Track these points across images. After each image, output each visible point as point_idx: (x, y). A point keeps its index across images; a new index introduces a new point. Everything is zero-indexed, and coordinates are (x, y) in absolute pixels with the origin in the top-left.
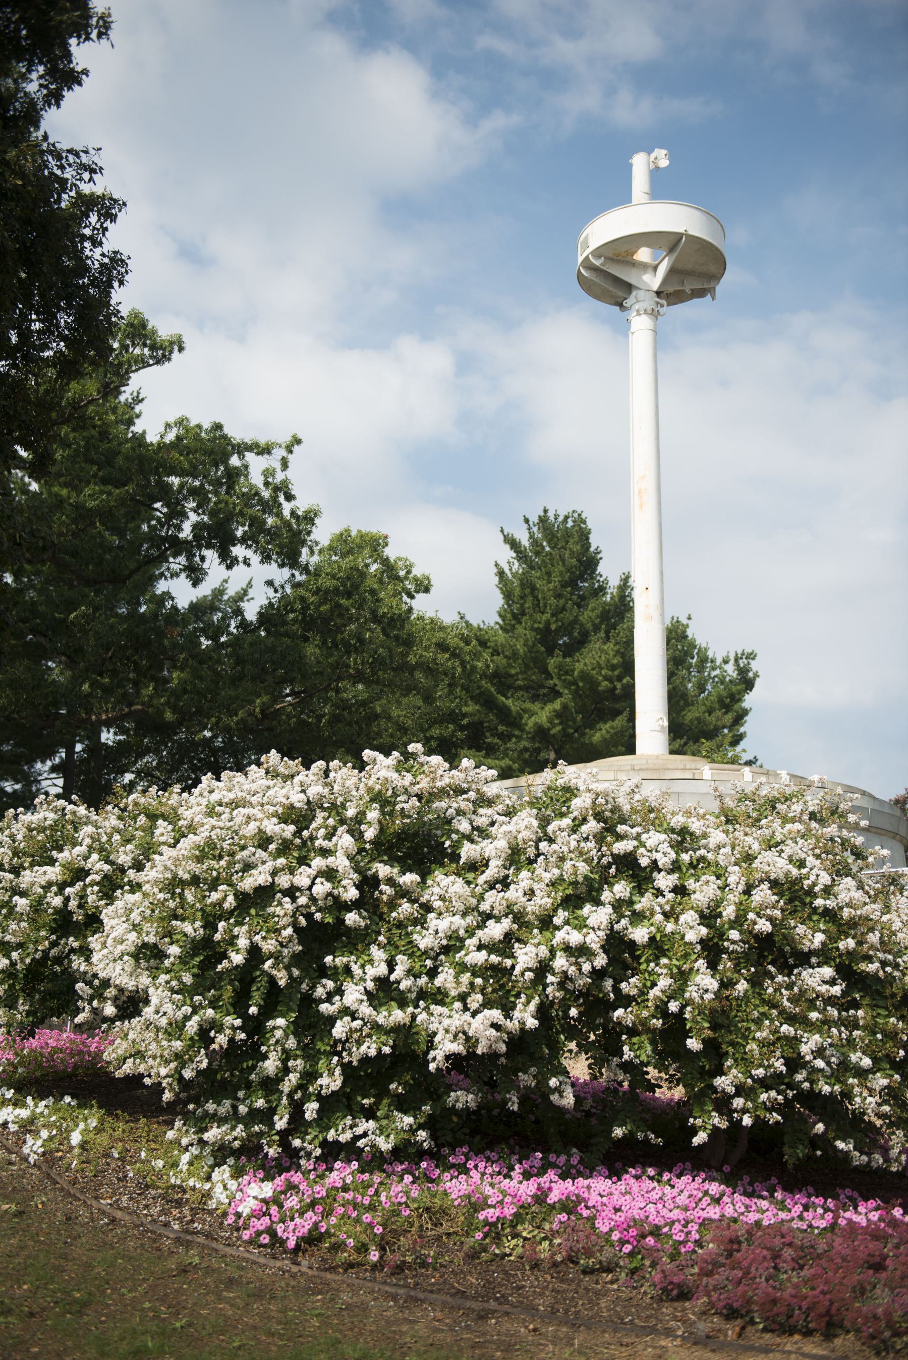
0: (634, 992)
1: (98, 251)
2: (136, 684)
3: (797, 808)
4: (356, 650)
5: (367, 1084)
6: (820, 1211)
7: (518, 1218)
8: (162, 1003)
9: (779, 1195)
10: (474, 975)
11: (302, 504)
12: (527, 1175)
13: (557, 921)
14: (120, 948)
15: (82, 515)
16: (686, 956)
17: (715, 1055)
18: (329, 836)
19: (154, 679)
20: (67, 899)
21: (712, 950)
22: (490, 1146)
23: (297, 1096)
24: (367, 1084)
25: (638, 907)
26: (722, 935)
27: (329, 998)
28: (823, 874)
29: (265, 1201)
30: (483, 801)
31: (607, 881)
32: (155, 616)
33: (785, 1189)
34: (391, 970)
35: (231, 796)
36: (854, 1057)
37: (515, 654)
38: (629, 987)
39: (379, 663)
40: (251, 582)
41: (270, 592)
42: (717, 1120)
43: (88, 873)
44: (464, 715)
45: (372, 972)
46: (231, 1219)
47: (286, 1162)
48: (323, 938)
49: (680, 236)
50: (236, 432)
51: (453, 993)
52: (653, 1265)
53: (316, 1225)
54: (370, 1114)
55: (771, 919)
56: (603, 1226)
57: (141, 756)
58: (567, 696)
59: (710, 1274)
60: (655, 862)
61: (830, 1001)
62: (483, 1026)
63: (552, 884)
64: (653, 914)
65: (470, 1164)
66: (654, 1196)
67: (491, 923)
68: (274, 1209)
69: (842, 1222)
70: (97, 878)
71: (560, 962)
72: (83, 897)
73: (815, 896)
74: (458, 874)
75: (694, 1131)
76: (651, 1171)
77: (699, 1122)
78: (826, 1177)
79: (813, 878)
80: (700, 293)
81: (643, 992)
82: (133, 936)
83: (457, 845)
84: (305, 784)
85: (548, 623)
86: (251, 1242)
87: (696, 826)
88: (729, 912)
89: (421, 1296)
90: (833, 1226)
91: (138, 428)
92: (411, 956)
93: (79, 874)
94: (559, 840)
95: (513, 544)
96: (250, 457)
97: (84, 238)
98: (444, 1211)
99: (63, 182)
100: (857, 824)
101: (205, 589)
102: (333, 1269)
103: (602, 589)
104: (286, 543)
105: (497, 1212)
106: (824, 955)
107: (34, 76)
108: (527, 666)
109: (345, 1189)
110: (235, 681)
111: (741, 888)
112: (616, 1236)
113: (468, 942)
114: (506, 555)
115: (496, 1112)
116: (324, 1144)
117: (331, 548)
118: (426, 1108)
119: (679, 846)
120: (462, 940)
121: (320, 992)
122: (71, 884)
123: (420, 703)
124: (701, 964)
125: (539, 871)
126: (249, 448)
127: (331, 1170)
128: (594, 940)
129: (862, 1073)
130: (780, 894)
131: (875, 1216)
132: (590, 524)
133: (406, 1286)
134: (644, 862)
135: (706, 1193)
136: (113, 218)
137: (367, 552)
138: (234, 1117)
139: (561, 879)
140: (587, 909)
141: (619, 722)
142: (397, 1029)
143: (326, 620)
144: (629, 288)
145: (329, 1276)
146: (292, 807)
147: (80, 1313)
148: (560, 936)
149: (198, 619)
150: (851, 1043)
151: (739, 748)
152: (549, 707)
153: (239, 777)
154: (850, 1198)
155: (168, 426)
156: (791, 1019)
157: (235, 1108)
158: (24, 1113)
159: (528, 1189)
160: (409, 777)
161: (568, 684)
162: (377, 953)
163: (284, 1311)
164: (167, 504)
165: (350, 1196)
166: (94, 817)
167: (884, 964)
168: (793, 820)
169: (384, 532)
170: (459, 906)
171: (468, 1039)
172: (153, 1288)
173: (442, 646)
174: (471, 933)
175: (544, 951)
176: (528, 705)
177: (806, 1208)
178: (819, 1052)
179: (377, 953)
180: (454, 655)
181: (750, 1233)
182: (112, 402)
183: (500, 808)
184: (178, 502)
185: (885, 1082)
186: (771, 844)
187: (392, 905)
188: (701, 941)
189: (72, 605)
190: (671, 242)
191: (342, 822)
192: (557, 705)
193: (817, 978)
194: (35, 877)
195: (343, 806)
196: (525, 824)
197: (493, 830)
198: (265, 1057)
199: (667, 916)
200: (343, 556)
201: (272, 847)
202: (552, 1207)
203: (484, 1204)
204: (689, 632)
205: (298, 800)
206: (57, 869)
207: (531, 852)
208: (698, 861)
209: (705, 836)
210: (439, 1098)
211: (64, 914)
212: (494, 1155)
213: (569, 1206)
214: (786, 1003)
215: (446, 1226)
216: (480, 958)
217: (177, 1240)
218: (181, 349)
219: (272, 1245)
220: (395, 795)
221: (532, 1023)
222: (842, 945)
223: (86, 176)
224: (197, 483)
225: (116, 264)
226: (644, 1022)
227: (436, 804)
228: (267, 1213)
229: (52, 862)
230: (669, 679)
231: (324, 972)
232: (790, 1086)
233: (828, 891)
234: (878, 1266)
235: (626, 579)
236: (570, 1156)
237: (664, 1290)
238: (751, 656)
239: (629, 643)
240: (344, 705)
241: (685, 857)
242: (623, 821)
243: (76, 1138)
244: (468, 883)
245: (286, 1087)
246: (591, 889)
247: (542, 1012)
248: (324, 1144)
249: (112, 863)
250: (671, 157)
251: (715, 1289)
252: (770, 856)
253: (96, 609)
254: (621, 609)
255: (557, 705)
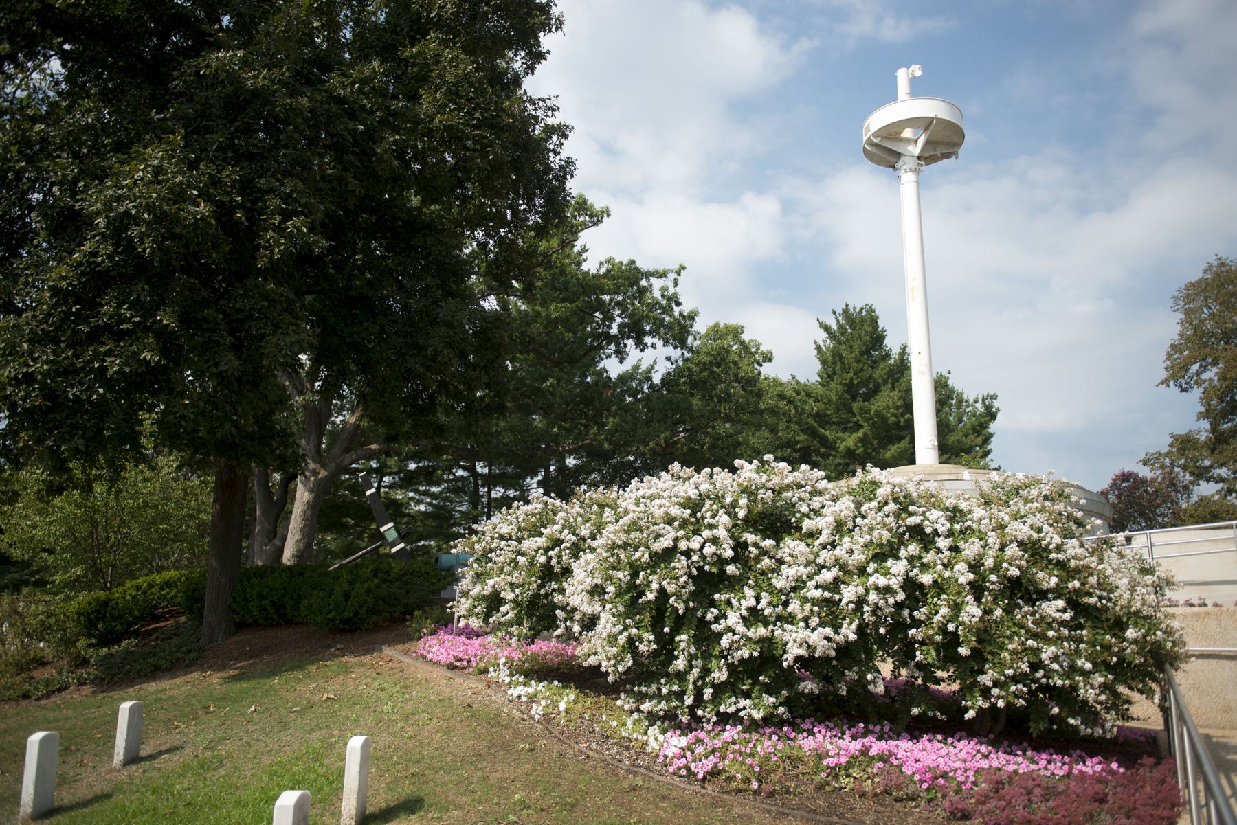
0: (923, 618)
1: (558, 157)
2: (586, 426)
3: (1035, 492)
4: (725, 401)
5: (746, 675)
6: (1059, 764)
7: (849, 765)
8: (606, 624)
9: (1029, 753)
10: (813, 605)
11: (686, 308)
12: (854, 738)
13: (869, 570)
14: (582, 587)
15: (551, 323)
16: (959, 593)
17: (979, 659)
18: (713, 517)
19: (596, 423)
20: (551, 558)
21: (977, 589)
22: (828, 718)
23: (699, 683)
24: (746, 675)
25: (925, 560)
26: (984, 579)
27: (717, 620)
28: (1055, 536)
29: (682, 748)
30: (817, 492)
31: (902, 543)
32: (596, 383)
33: (1033, 750)
34: (758, 602)
35: (650, 492)
36: (1079, 663)
37: (830, 401)
38: (921, 614)
39: (739, 407)
40: (656, 359)
41: (668, 364)
42: (981, 702)
43: (562, 542)
44: (797, 443)
45: (745, 604)
46: (661, 759)
47: (694, 725)
48: (710, 582)
49: (932, 119)
50: (643, 265)
51: (800, 616)
52: (944, 797)
53: (716, 765)
54: (747, 695)
55: (1019, 567)
56: (908, 771)
57: (590, 473)
58: (866, 428)
59: (984, 803)
60: (936, 530)
61: (1063, 623)
62: (819, 639)
63: (866, 546)
64: (935, 565)
65: (816, 730)
66: (943, 752)
67: (824, 571)
68: (688, 754)
69: (1075, 772)
70: (568, 545)
71: (873, 597)
72: (559, 557)
73: (1050, 552)
74: (801, 540)
75: (966, 710)
76: (939, 737)
77: (969, 703)
78: (1062, 741)
79: (1048, 539)
80: (947, 156)
81: (929, 618)
82: (589, 580)
83: (799, 521)
84: (698, 482)
85: (852, 379)
86: (674, 774)
87: (963, 506)
88: (989, 562)
89: (787, 811)
90: (1069, 775)
91: (585, 267)
92: (771, 593)
93: (557, 542)
94: (869, 517)
95: (826, 328)
96: (653, 280)
97: (549, 151)
98: (800, 759)
99: (536, 118)
100: (1077, 503)
101: (627, 366)
102: (728, 793)
103: (888, 355)
104: (678, 333)
105: (835, 760)
106: (1058, 592)
107: (519, 58)
108: (838, 409)
109: (734, 743)
110: (648, 423)
111: (997, 546)
112: (917, 777)
113: (808, 583)
114: (821, 336)
115: (830, 698)
116: (718, 714)
117: (707, 335)
118: (784, 692)
119: (952, 520)
120: (804, 582)
121: (709, 617)
122: (553, 549)
123: (769, 435)
124: (970, 598)
125: (856, 537)
126: (653, 274)
127: (724, 731)
128: (895, 583)
129: (1085, 674)
130: (1026, 551)
131: (1098, 768)
132: (878, 312)
133: (777, 805)
134: (928, 530)
135: (978, 751)
136: (566, 136)
137: (730, 337)
138: (658, 696)
139: (871, 542)
140: (890, 562)
141: (903, 444)
142: (762, 640)
143: (705, 382)
144: (898, 155)
145: (725, 796)
146: (690, 498)
147: (571, 811)
148: (872, 580)
149: (623, 385)
150: (1077, 653)
151: (988, 459)
152: (855, 435)
153: (655, 480)
154: (1080, 757)
155: (601, 263)
156: (1035, 636)
157: (659, 690)
158: (530, 690)
159: (855, 746)
160: (765, 477)
161: (867, 420)
162: (748, 592)
163: (698, 816)
164: (601, 313)
165: (739, 747)
166: (565, 507)
167: (1100, 598)
168: (1032, 501)
169: (741, 324)
170: (802, 560)
171: (809, 647)
172: (615, 798)
173: (781, 396)
174: (810, 578)
175: (861, 590)
176: (840, 434)
177: (1049, 762)
178: (1055, 659)
179: (748, 592)
180: (790, 402)
181: (1010, 777)
182: (567, 251)
183: (828, 496)
184: (609, 311)
185: (1102, 680)
186: (1017, 517)
187: (757, 560)
188: (970, 583)
189: (544, 379)
190: (926, 124)
191: (722, 507)
192: (860, 434)
193: (1053, 608)
194: (530, 544)
195: (723, 497)
196: (845, 506)
197: (824, 511)
198: (677, 658)
199: (945, 566)
200: (715, 340)
201: (676, 524)
202: (873, 758)
203: (826, 755)
204: (950, 382)
205: (693, 493)
206: (544, 539)
207: (850, 525)
208: (966, 529)
209: (970, 512)
210: (793, 686)
211: (547, 567)
212: (831, 725)
213: (884, 758)
214: (1031, 625)
215: (801, 769)
216: (817, 593)
217: (628, 770)
218: (608, 215)
219: (688, 777)
220: (757, 489)
221: (852, 637)
222: (1070, 585)
223: (550, 113)
224: (621, 298)
225: (568, 166)
226: (930, 638)
227: (785, 494)
228: (684, 756)
229: (541, 535)
230: (938, 412)
231: (713, 604)
232: (1034, 681)
233: (1059, 548)
234: (1102, 800)
235: (904, 348)
236: (883, 726)
237: (952, 813)
238: (994, 397)
239: (909, 391)
240: (717, 437)
241: (957, 527)
242: (913, 504)
243: (562, 706)
244: (808, 545)
245: (691, 678)
246: (892, 549)
247: (861, 630)
248: (718, 714)
249: (577, 535)
250: (923, 69)
251: (987, 813)
252: (1017, 525)
253: (559, 380)
254: (902, 369)
255: (860, 434)
